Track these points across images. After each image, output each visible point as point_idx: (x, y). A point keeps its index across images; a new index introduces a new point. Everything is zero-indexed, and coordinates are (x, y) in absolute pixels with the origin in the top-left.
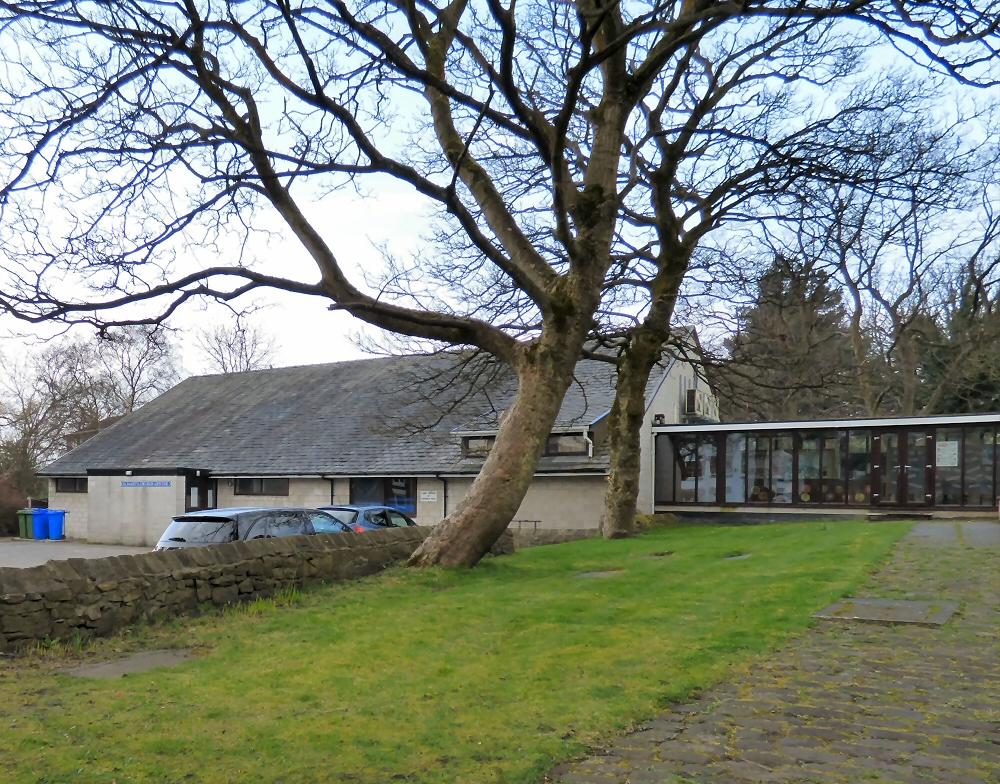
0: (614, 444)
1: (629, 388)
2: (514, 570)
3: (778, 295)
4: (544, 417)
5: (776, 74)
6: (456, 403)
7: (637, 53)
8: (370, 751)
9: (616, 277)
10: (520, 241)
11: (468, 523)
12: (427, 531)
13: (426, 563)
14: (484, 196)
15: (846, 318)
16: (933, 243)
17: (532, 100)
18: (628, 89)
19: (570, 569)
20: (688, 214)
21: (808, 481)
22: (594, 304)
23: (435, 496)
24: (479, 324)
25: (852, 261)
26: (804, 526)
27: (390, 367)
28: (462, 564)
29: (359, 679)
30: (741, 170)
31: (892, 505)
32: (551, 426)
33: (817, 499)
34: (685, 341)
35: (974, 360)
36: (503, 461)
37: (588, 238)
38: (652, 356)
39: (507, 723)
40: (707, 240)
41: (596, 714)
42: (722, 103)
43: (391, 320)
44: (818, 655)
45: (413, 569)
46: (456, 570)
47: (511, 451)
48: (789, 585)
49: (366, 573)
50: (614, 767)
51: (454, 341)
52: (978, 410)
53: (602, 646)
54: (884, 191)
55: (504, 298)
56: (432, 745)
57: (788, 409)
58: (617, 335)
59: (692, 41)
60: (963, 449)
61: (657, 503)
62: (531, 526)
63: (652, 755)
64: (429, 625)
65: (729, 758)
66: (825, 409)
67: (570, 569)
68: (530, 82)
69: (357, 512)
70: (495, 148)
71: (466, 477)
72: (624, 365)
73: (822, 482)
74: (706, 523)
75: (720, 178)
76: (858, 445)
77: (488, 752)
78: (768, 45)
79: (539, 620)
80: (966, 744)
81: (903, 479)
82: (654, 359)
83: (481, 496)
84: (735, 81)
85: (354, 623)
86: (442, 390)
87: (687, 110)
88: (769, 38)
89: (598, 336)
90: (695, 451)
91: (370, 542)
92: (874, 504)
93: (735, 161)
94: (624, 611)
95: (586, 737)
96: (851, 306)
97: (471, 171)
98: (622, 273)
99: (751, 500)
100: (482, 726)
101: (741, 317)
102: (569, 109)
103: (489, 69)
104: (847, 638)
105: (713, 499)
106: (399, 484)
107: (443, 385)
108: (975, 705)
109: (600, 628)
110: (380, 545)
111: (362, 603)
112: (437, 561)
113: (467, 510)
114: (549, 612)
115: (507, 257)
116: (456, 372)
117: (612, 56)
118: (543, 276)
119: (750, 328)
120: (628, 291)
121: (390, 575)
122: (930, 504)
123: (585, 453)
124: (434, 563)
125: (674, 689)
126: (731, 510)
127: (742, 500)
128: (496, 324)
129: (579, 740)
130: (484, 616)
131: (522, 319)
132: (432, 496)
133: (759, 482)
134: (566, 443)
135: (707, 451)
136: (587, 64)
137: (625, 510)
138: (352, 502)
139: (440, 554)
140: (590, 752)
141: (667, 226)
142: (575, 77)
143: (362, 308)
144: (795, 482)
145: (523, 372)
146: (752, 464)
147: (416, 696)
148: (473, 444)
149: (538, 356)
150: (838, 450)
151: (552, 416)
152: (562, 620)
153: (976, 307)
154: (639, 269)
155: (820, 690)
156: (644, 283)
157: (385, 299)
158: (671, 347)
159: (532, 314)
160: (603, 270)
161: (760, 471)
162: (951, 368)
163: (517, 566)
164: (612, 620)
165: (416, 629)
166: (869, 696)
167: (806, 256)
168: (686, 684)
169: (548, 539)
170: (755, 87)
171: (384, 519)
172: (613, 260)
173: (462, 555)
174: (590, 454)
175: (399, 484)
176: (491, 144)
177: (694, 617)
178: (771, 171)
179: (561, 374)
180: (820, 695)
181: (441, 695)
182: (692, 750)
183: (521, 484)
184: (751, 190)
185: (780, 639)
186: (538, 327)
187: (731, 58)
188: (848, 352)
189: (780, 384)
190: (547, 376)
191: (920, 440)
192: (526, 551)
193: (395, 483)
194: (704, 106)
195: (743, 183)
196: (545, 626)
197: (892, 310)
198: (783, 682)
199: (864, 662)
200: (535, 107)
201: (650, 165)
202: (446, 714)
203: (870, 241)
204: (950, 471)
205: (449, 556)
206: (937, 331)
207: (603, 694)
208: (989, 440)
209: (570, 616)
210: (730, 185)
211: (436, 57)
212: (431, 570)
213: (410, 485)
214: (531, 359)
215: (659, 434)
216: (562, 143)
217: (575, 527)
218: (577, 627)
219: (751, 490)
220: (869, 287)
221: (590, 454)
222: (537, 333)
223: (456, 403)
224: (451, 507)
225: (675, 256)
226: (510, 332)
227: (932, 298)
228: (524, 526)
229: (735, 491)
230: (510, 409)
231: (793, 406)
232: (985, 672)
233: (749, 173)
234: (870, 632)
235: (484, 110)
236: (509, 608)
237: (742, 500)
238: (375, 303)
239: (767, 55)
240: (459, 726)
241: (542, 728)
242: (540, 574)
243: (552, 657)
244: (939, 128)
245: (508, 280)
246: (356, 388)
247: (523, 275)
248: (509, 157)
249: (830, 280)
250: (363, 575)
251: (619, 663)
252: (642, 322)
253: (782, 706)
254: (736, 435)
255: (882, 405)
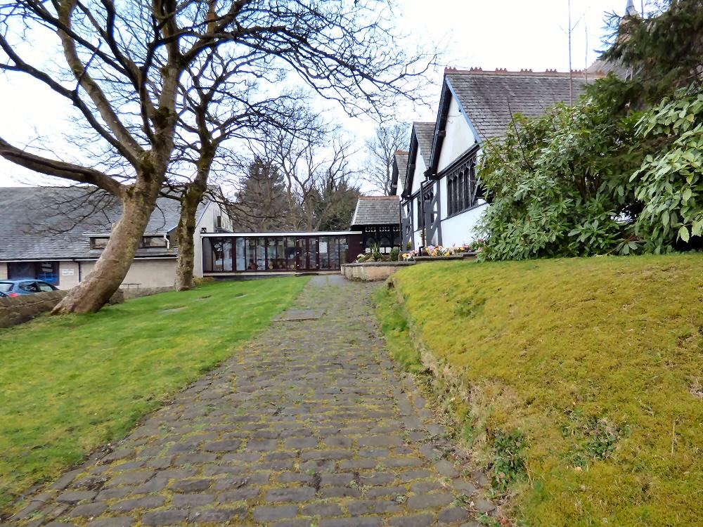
0: (180, 242)
1: (187, 214)
2: (123, 312)
3: (257, 174)
4: (138, 227)
5: (253, 73)
6: (85, 217)
7: (186, 44)
8: (15, 436)
9: (179, 156)
10: (123, 131)
11: (92, 287)
12: (65, 293)
13: (64, 313)
14: (99, 101)
15: (285, 188)
16: (316, 160)
17: (128, 54)
18: (181, 61)
19: (157, 309)
20: (214, 130)
21: (272, 260)
22: (165, 170)
23: (72, 272)
24: (98, 173)
25: (287, 163)
26: (270, 280)
27: (38, 193)
28: (90, 311)
29: (9, 392)
30: (239, 114)
31: (304, 269)
32: (143, 233)
33: (276, 268)
34: (214, 193)
35: (332, 209)
36: (114, 251)
37: (161, 134)
38: (198, 198)
39: (114, 399)
40: (223, 144)
41: (167, 384)
42: (229, 80)
43: (34, 164)
44: (272, 338)
45: (55, 317)
46: (85, 315)
47: (120, 246)
48: (262, 307)
49: (18, 323)
50: (176, 409)
51: (82, 181)
52: (334, 230)
53: (172, 348)
54: (297, 134)
55: (115, 159)
56: (63, 422)
57: (263, 227)
58: (180, 186)
59: (214, 46)
60: (328, 246)
61: (204, 272)
62: (135, 287)
63: (195, 399)
64: (65, 350)
65: (232, 393)
66: (279, 227)
67: (157, 309)
68: (127, 43)
69: (13, 284)
70: (107, 75)
71: (92, 260)
72: (184, 202)
73: (277, 260)
74: (229, 281)
75: (228, 116)
76: (291, 244)
77: (101, 417)
78: (249, 58)
79: (138, 338)
80: (325, 366)
81: (308, 258)
82: (199, 200)
83: (101, 271)
84: (234, 71)
85: (7, 355)
86: (75, 209)
87: (213, 79)
88: (249, 56)
89: (169, 186)
90: (222, 246)
91: (21, 303)
92: (298, 269)
93: (235, 109)
94: (184, 327)
95: (160, 397)
96: (287, 183)
97: (90, 84)
98: (182, 155)
99: (248, 269)
100: (97, 404)
101: (242, 183)
102: (149, 63)
103: (101, 30)
104: (284, 329)
105: (231, 269)
106: (48, 265)
107: (75, 206)
108: (329, 350)
109: (171, 338)
110: (30, 304)
111: (14, 342)
112: (72, 311)
113: (92, 280)
114: (143, 333)
115: (115, 137)
116: (84, 199)
117: (172, 40)
118: (136, 150)
119: (247, 188)
120: (186, 164)
121: (38, 322)
122: (318, 269)
123: (165, 247)
124: (70, 312)
125: (207, 364)
126: (239, 274)
127: (244, 269)
128: (109, 173)
129: (157, 400)
130: (103, 340)
131: (125, 173)
132: (70, 272)
133: (251, 261)
134: (155, 241)
135: (227, 246)
136: (158, 43)
137: (187, 276)
138: (9, 277)
139: (74, 306)
140: (163, 404)
141: (205, 135)
142: (152, 48)
143: (18, 156)
144: (266, 260)
145: (125, 201)
146: (248, 252)
147: (54, 394)
148: (98, 242)
149: (134, 194)
150: (283, 246)
151: (143, 227)
152: (150, 337)
153: (332, 188)
154: (191, 154)
155: (272, 353)
156: (193, 161)
157: (28, 150)
158: (208, 194)
159: (131, 171)
160: (169, 152)
161: (251, 256)
162: (324, 212)
163: (126, 309)
164: (178, 334)
165: (55, 354)
166: (291, 352)
167: (269, 158)
168: (213, 360)
169: (146, 293)
170: (244, 76)
171: (35, 288)
172: (175, 147)
173: (89, 307)
174: (168, 247)
175: (48, 265)
176: (99, 72)
177: (219, 327)
178: (252, 117)
179: (148, 204)
180: (273, 356)
181: (71, 390)
182: (215, 393)
183: (126, 263)
184: (243, 124)
185: (257, 333)
186: (135, 177)
187: (232, 60)
188: (287, 202)
189: (259, 216)
190: (139, 204)
191: (314, 242)
192: (133, 301)
193: (44, 265)
194: (220, 80)
195: (239, 120)
196: (141, 341)
197: (303, 186)
198: (257, 352)
199: (290, 338)
200: (130, 59)
201: (196, 103)
202: (74, 401)
203: (293, 156)
204: (324, 255)
205: (80, 307)
206: (319, 196)
207: (170, 373)
208: (337, 241)
209: (154, 334)
210: (233, 120)
211: (65, 14)
212: (68, 316)
213: (55, 265)
214: (130, 195)
215: (204, 237)
216: (145, 79)
217: (161, 286)
218: (159, 339)
219: (248, 265)
220: (294, 175)
221: (168, 247)
222: (134, 181)
223: (85, 217)
224: (83, 279)
225: (208, 151)
226: (118, 179)
227: (317, 182)
228: (131, 287)
229: (241, 265)
230: (119, 221)
231: (265, 226)
232: (333, 336)
233: (242, 116)
234: (293, 325)
235: (97, 52)
236: (119, 333)
237: (244, 269)
238: (22, 152)
239: (248, 63)
240: (83, 406)
241: (135, 398)
242: (139, 313)
243: (143, 358)
244: (315, 112)
245: (116, 150)
246: (11, 205)
247: (124, 148)
248: (116, 82)
249: (279, 170)
250: (16, 324)
251: (181, 355)
252: (193, 181)
253: (257, 363)
254: (241, 239)
255: (300, 226)
